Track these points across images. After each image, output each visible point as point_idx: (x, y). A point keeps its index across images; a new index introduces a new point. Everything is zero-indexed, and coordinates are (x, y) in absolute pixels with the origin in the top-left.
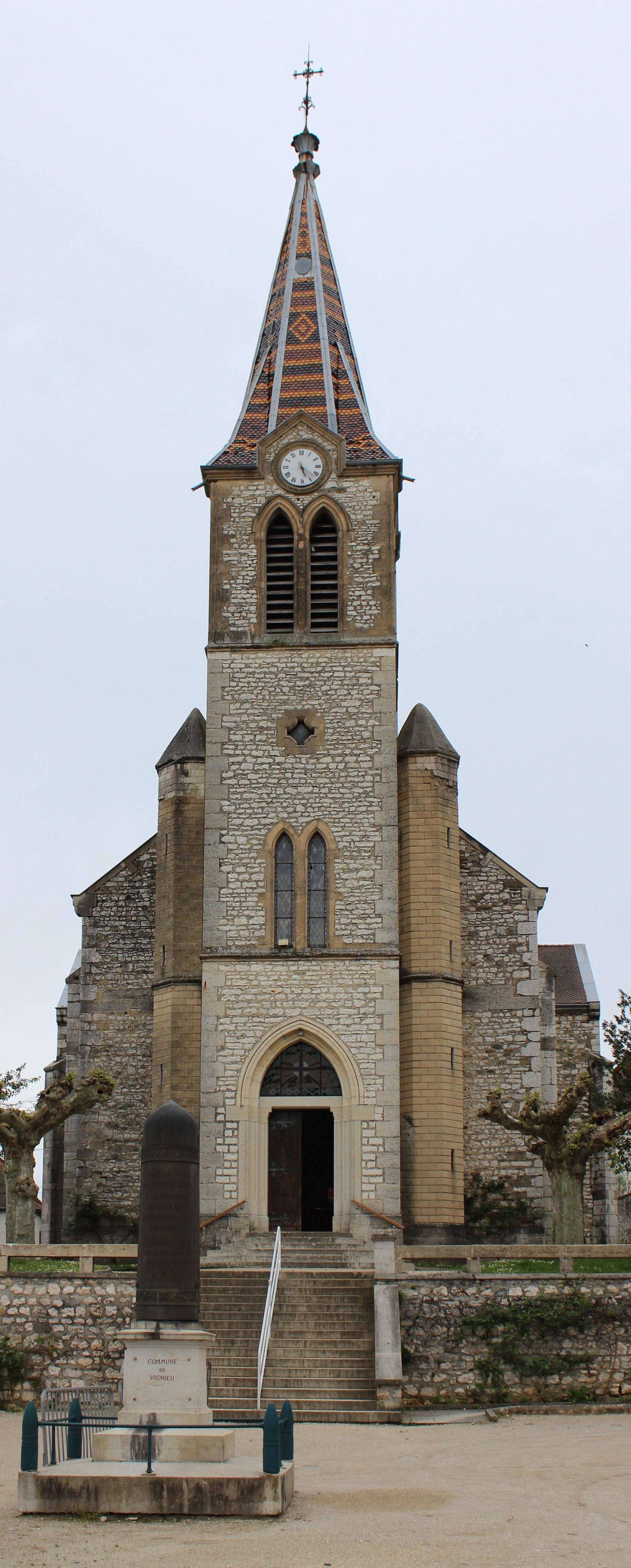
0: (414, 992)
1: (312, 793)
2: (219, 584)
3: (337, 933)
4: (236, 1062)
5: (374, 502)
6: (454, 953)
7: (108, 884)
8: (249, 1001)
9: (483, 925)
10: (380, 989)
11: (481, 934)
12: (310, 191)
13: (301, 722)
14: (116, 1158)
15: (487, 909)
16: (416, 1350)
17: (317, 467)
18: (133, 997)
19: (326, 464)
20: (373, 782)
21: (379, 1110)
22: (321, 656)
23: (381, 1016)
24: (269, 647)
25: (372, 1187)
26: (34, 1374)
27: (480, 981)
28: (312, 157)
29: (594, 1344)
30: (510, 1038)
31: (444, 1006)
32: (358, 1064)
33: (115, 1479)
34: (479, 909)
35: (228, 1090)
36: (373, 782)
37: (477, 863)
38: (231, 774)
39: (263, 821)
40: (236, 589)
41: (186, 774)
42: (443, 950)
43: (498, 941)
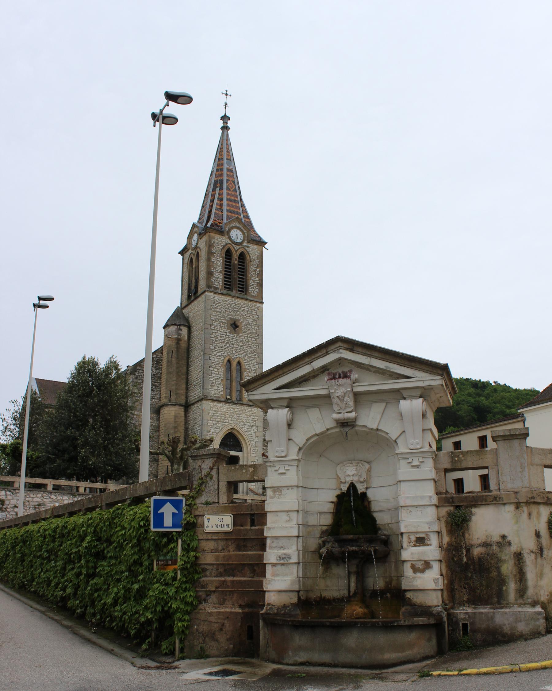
2: (259, 280)
8: (218, 416)
13: (234, 323)
19: (244, 237)
21: (257, 458)
23: (258, 427)
41: (181, 330)
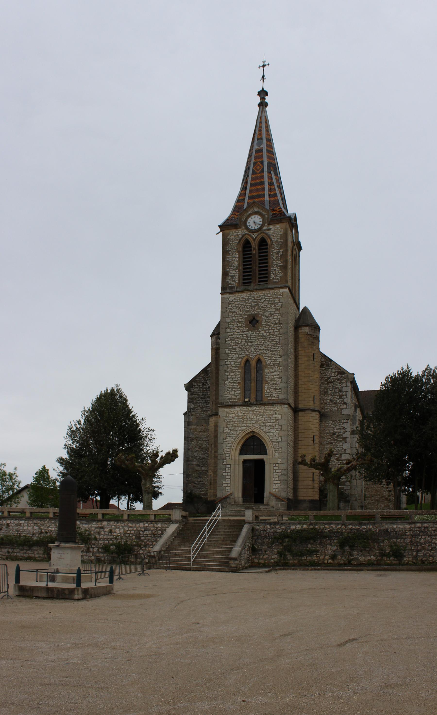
0: (300, 415)
1: (257, 344)
3: (266, 396)
4: (230, 444)
5: (281, 233)
6: (315, 400)
7: (197, 379)
8: (235, 422)
9: (330, 389)
10: (281, 416)
11: (329, 392)
12: (263, 113)
13: (254, 318)
14: (199, 477)
15: (331, 382)
16: (258, 547)
17: (260, 221)
18: (205, 420)
20: (279, 339)
21: (280, 460)
22: (261, 293)
24: (242, 292)
25: (277, 487)
26: (135, 553)
27: (328, 410)
28: (265, 99)
29: (319, 546)
30: (339, 431)
31: (310, 420)
32: (273, 443)
33: (37, 587)
34: (328, 383)
35: (227, 453)
36: (279, 339)
37: (328, 365)
38: (229, 339)
39: (240, 356)
40: (231, 270)
42: (311, 399)
43: (335, 394)
